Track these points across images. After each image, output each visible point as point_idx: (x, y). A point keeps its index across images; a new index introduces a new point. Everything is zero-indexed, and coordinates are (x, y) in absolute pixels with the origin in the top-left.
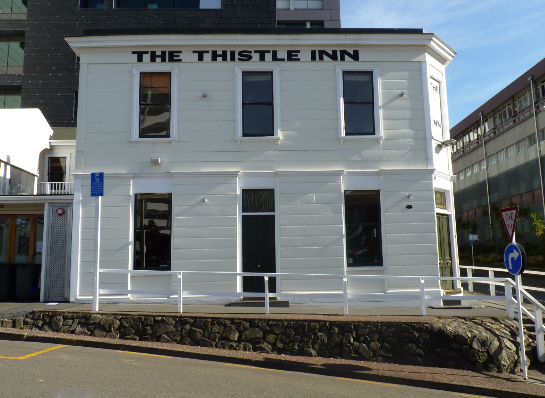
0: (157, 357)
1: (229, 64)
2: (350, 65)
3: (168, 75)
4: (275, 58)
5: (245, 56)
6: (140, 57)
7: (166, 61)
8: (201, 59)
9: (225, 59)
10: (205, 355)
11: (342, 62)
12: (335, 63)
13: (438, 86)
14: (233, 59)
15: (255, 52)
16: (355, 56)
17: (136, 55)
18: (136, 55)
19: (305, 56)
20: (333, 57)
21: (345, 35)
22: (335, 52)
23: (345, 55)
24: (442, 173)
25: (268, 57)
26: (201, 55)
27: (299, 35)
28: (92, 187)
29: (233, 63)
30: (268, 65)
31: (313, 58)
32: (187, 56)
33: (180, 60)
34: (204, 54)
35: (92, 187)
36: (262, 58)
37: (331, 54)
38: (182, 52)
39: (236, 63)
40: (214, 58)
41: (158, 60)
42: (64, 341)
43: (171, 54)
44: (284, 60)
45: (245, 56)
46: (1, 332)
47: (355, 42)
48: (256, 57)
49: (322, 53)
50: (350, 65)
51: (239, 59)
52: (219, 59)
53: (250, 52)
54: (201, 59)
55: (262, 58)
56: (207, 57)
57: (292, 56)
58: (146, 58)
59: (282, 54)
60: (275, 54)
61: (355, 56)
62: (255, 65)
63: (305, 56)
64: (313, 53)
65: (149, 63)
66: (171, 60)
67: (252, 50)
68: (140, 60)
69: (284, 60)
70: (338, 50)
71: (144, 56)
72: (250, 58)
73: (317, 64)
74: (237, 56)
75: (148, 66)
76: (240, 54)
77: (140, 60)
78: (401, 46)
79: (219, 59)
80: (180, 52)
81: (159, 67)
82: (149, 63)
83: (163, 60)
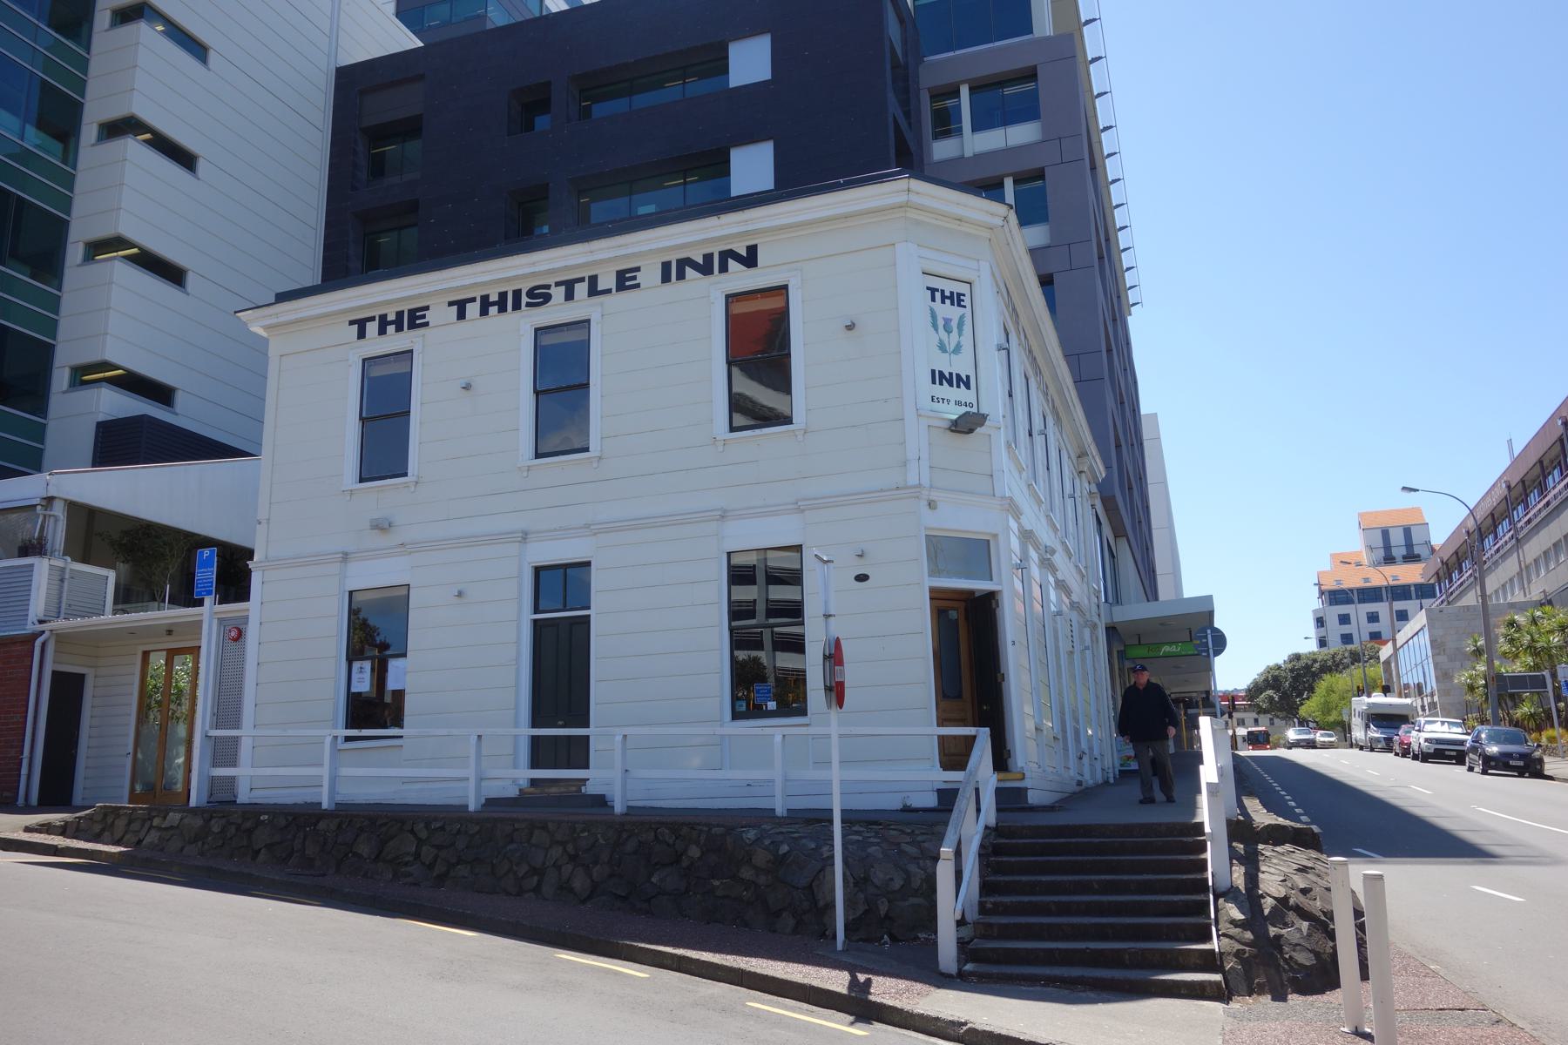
0: (430, 928)
1: (511, 316)
2: (740, 279)
3: (408, 354)
4: (593, 291)
5: (539, 296)
6: (361, 325)
7: (506, 311)
8: (461, 315)
9: (502, 309)
10: (812, 988)
11: (724, 276)
12: (711, 279)
13: (968, 295)
14: (517, 306)
15: (558, 284)
16: (750, 259)
17: (455, 308)
18: (455, 308)
19: (441, 314)
20: (705, 268)
21: (715, 217)
22: (708, 258)
23: (731, 261)
24: (670, 516)
25: (581, 290)
26: (461, 307)
27: (294, 301)
28: (1413, 588)
29: (517, 314)
30: (582, 306)
31: (666, 278)
32: (441, 314)
33: (638, 286)
34: (467, 305)
35: (1413, 588)
36: (569, 296)
37: (745, 255)
38: (642, 269)
39: (523, 313)
40: (484, 312)
41: (391, 329)
42: (104, 856)
43: (412, 312)
44: (609, 291)
45: (539, 296)
46: (3, 835)
47: (591, 258)
48: (558, 293)
49: (684, 263)
50: (740, 279)
51: (528, 305)
52: (493, 310)
53: (548, 287)
54: (461, 315)
55: (569, 296)
56: (473, 309)
57: (625, 280)
58: (372, 328)
59: (607, 281)
60: (593, 280)
61: (750, 259)
62: (557, 311)
63: (649, 275)
64: (666, 267)
65: (658, 286)
66: (412, 326)
67: (551, 281)
68: (362, 334)
69: (609, 291)
70: (716, 250)
71: (469, 306)
72: (547, 298)
73: (675, 287)
74: (525, 299)
75: (377, 344)
76: (531, 294)
77: (362, 334)
78: (846, 217)
79: (493, 310)
80: (427, 308)
81: (394, 341)
82: (658, 286)
83: (399, 329)
